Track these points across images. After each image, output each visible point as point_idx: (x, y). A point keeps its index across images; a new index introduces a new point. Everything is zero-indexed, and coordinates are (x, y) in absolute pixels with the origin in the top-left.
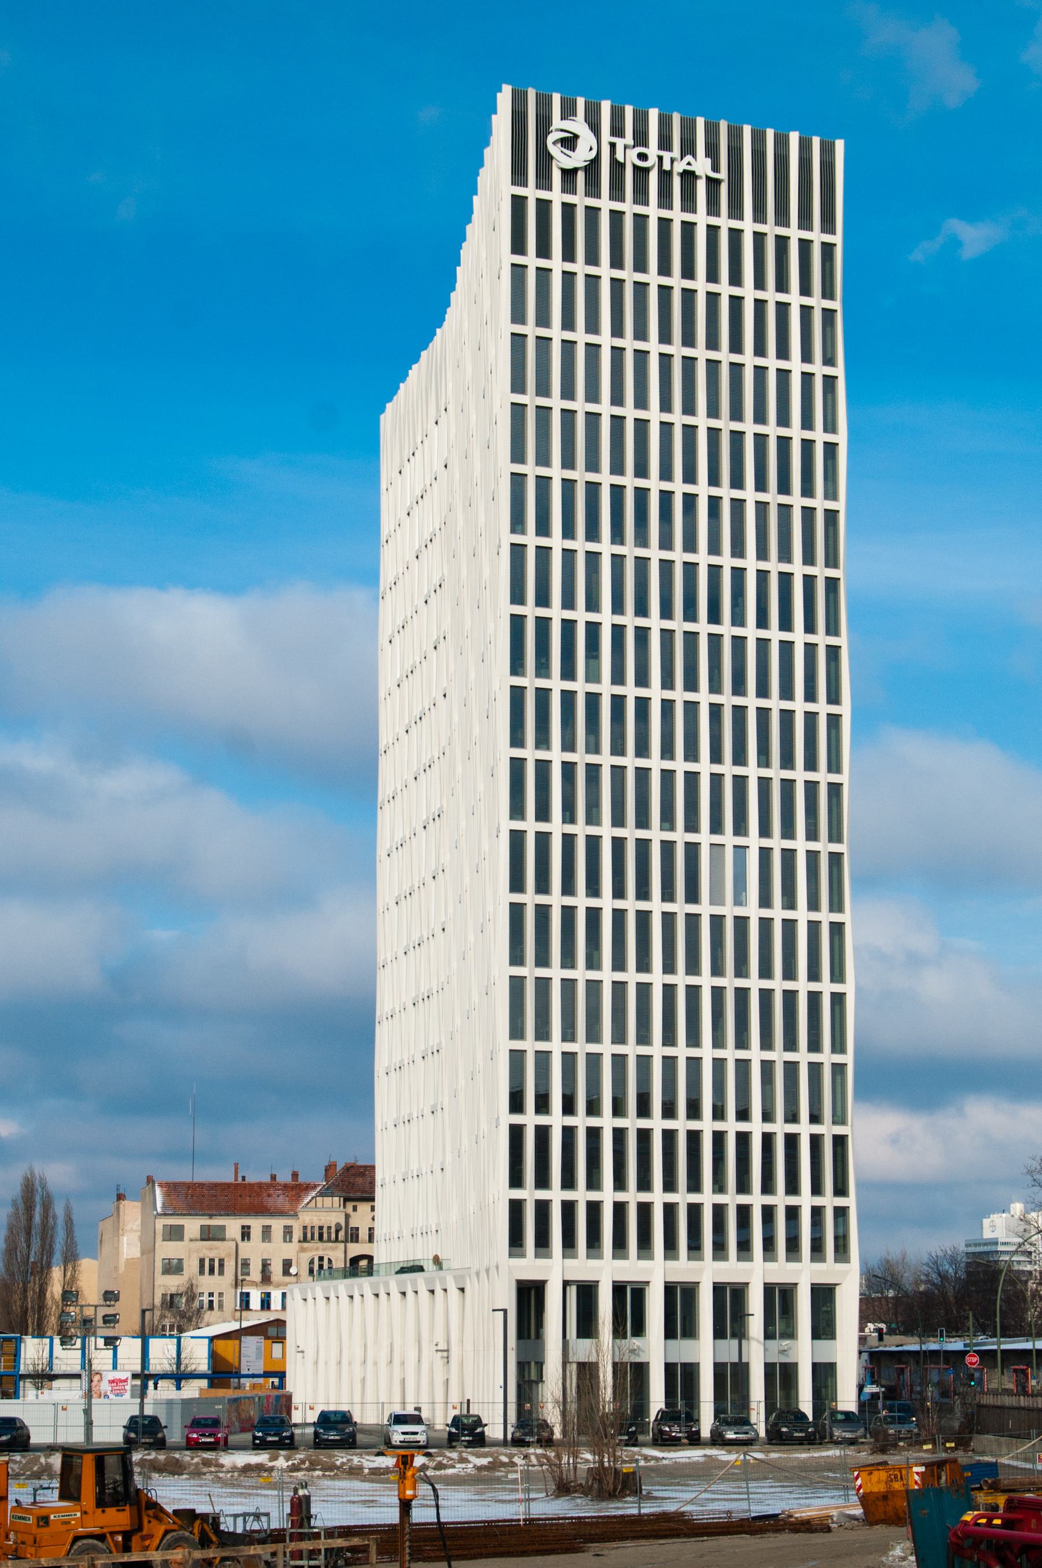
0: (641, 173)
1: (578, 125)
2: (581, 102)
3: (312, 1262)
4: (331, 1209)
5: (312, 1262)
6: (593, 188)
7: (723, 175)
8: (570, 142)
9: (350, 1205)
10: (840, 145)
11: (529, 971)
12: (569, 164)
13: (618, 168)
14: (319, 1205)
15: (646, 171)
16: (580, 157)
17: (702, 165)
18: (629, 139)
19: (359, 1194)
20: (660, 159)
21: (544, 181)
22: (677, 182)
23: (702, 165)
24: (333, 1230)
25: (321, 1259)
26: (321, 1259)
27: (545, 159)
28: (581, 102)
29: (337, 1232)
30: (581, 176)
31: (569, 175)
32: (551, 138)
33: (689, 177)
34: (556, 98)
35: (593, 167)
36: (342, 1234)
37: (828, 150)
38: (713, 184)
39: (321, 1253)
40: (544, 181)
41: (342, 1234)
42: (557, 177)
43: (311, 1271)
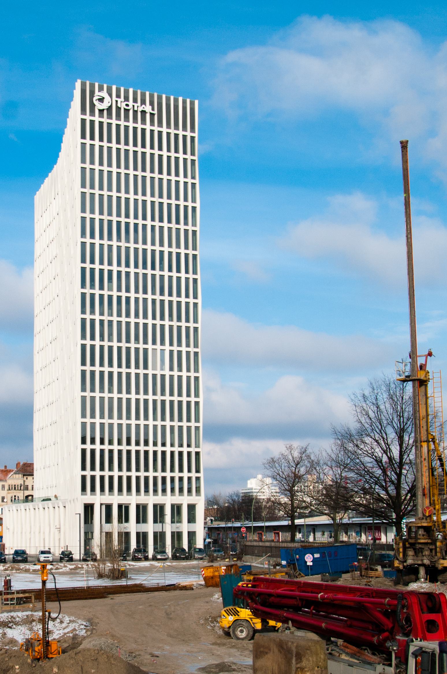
0: (127, 111)
1: (104, 94)
2: (105, 86)
3: (12, 497)
4: (19, 479)
5: (12, 497)
6: (110, 116)
7: (156, 112)
8: (101, 100)
9: (25, 477)
10: (196, 102)
11: (88, 368)
12: (101, 108)
13: (118, 109)
14: (14, 477)
15: (129, 110)
16: (105, 105)
17: (148, 108)
18: (122, 99)
19: (28, 473)
20: (133, 106)
21: (92, 113)
22: (139, 114)
23: (148, 108)
24: (19, 486)
25: (15, 496)
26: (15, 496)
27: (92, 106)
28: (105, 86)
29: (21, 487)
30: (105, 112)
31: (101, 111)
32: (95, 99)
33: (143, 112)
34: (97, 85)
35: (110, 109)
36: (22, 488)
37: (192, 104)
38: (152, 115)
39: (15, 494)
40: (92, 113)
41: (22, 488)
42: (97, 112)
43: (12, 501)
